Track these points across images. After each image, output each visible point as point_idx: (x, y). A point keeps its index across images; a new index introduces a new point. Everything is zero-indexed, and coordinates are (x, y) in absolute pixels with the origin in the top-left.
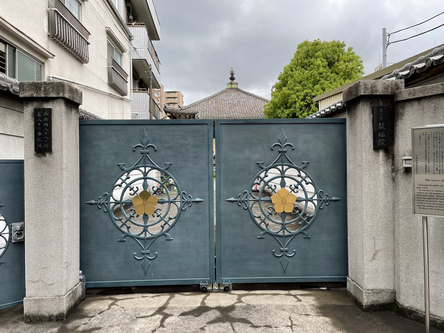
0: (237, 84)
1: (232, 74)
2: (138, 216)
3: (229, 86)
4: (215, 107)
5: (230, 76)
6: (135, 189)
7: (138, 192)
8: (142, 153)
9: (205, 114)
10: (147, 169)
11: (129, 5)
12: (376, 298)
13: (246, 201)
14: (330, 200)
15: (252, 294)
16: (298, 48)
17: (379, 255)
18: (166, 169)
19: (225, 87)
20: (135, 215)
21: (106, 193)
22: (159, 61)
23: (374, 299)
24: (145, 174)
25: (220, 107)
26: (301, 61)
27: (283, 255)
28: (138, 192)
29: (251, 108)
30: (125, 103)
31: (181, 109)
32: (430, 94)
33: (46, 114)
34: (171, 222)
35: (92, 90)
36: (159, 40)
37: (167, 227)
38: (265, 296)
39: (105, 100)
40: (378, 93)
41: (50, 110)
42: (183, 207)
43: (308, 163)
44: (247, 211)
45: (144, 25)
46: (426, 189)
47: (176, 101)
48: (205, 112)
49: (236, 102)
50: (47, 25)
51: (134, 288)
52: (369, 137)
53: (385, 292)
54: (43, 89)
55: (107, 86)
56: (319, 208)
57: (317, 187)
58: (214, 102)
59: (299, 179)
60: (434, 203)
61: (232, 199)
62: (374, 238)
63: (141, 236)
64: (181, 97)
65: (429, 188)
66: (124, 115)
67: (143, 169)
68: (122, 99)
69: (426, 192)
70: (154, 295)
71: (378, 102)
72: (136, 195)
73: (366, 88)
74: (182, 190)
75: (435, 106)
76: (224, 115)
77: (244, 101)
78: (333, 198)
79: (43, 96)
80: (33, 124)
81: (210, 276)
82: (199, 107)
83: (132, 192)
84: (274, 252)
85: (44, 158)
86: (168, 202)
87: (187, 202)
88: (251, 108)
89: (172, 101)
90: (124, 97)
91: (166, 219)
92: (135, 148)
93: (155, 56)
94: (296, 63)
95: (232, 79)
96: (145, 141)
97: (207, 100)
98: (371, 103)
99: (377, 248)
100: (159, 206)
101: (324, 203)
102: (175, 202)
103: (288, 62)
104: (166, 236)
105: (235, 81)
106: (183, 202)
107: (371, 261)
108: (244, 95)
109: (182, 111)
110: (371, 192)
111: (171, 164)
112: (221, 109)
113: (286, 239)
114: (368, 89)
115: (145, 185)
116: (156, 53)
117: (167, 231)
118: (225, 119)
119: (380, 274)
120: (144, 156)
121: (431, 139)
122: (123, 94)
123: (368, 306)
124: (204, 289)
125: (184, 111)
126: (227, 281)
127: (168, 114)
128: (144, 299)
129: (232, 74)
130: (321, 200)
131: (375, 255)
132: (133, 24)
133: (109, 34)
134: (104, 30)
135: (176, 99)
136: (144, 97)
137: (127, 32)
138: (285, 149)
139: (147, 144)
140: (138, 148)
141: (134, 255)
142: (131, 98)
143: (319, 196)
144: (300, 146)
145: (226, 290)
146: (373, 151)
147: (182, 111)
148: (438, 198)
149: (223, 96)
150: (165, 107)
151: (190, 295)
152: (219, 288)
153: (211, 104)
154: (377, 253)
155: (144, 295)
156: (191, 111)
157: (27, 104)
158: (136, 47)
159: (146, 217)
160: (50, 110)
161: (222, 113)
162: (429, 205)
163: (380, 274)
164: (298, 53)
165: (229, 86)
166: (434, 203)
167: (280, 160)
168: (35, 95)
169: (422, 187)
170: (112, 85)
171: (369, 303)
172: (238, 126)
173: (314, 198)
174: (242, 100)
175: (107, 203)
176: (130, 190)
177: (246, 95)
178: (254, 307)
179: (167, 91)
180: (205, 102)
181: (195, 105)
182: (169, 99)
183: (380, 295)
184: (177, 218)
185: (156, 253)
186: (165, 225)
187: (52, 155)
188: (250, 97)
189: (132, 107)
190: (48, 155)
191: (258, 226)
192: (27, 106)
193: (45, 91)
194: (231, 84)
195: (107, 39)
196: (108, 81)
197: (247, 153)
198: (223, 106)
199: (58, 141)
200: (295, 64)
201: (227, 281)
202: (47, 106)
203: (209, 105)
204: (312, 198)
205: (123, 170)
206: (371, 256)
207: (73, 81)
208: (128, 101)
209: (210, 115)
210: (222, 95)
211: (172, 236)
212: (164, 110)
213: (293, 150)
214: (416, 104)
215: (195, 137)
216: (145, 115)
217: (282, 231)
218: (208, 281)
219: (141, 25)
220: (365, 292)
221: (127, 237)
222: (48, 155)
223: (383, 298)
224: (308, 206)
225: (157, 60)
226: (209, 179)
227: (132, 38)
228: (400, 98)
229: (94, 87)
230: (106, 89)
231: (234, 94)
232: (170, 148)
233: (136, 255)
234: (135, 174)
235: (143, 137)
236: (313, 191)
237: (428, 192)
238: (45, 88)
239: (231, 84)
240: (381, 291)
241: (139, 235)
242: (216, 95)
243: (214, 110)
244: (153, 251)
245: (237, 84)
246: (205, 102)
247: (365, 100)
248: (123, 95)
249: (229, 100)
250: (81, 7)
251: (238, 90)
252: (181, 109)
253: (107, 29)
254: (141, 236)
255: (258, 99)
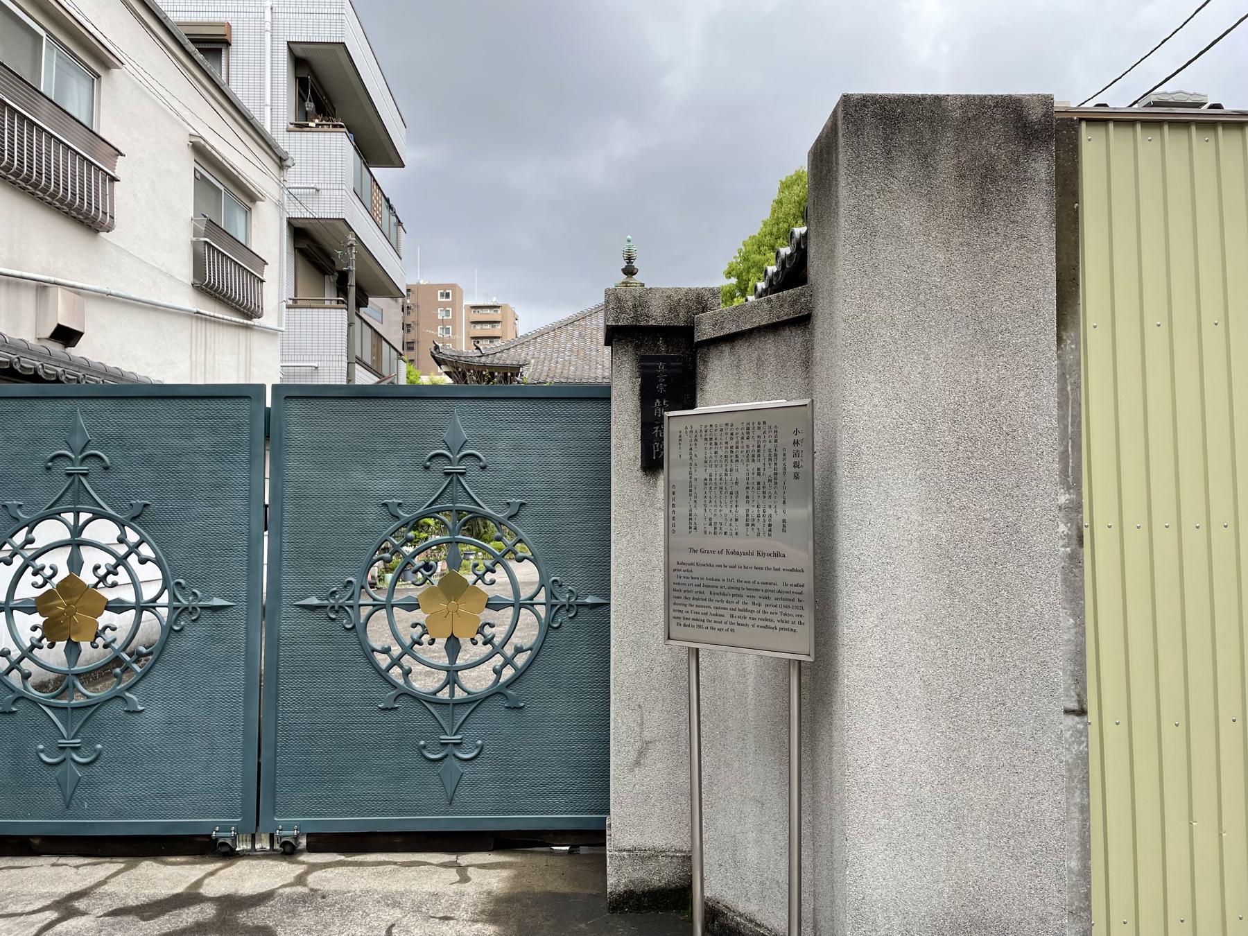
1: (629, 259)
2: (432, 642)
4: (575, 349)
6: (48, 572)
7: (56, 580)
8: (447, 474)
10: (84, 517)
11: (304, 74)
12: (641, 873)
13: (351, 607)
14: (579, 605)
15: (361, 864)
16: (781, 191)
17: (652, 755)
18: (510, 518)
20: (426, 638)
21: (350, 579)
22: (399, 223)
23: (636, 875)
24: (77, 530)
26: (786, 225)
27: (446, 756)
28: (56, 580)
30: (255, 338)
31: (483, 355)
32: (748, 327)
34: (521, 660)
35: (129, 304)
36: (403, 166)
37: (508, 673)
38: (380, 868)
39: (183, 331)
40: (652, 323)
42: (175, 623)
43: (522, 504)
44: (352, 635)
45: (341, 127)
46: (689, 574)
47: (497, 330)
51: (37, 842)
52: (631, 436)
53: (667, 856)
55: (189, 291)
56: (549, 625)
57: (543, 570)
58: (576, 334)
59: (122, 550)
60: (705, 610)
61: (314, 601)
62: (639, 706)
63: (440, 695)
64: (511, 320)
65: (697, 572)
66: (253, 369)
67: (69, 517)
68: (247, 327)
69: (690, 581)
70: (87, 860)
71: (655, 345)
72: (48, 587)
73: (620, 308)
74: (176, 575)
75: (759, 359)
76: (599, 371)
78: (589, 600)
81: (243, 814)
83: (39, 580)
84: (424, 747)
86: (513, 605)
87: (187, 608)
89: (487, 330)
90: (255, 322)
91: (509, 650)
92: (430, 460)
93: (386, 211)
94: (775, 230)
96: (78, 442)
97: (556, 329)
98: (637, 347)
99: (647, 735)
100: (488, 615)
101: (563, 611)
102: (532, 605)
103: (756, 229)
104: (125, 700)
105: (637, 278)
106: (176, 608)
107: (631, 770)
109: (483, 360)
110: (634, 581)
111: (146, 505)
113: (458, 710)
114: (625, 312)
115: (75, 564)
116: (388, 201)
117: (510, 684)
118: (599, 380)
119: (654, 805)
120: (73, 481)
121: (701, 441)
122: (248, 312)
123: (619, 895)
124: (225, 849)
125: (488, 361)
126: (288, 826)
127: (445, 368)
128: (54, 869)
129: (630, 259)
130: (554, 606)
131: (642, 753)
132: (311, 124)
133: (200, 151)
134: (184, 141)
135: (499, 326)
136: (331, 321)
137: (269, 146)
138: (461, 467)
139: (460, 450)
140: (59, 462)
141: (38, 752)
142: (280, 324)
143: (551, 595)
144: (502, 458)
145: (288, 851)
146: (640, 474)
147: (483, 360)
148: (712, 597)
150: (436, 347)
151: (181, 863)
152: (253, 845)
154: (647, 749)
155: (62, 860)
156: (508, 359)
158: (319, 186)
159: (453, 646)
161: (593, 365)
162: (763, 616)
163: (654, 805)
164: (780, 202)
166: (705, 610)
167: (447, 496)
169: (683, 567)
170: (205, 288)
171: (622, 888)
172: (331, 402)
173: (536, 600)
175: (351, 607)
176: (35, 574)
178: (324, 897)
179: (474, 304)
180: (551, 334)
182: (478, 327)
183: (652, 865)
184: (538, 651)
185: (99, 746)
186: (503, 666)
189: (291, 344)
191: (383, 675)
195: (194, 165)
196: (194, 276)
197: (359, 476)
200: (771, 234)
201: (289, 824)
204: (531, 599)
205: (17, 519)
206: (633, 755)
207: (53, 279)
208: (265, 331)
209: (559, 371)
211: (143, 701)
212: (434, 357)
213: (483, 468)
214: (726, 349)
215: (215, 431)
216: (333, 374)
217: (447, 690)
218: (237, 827)
219: (335, 126)
220: (611, 857)
221: (21, 703)
223: (660, 875)
224: (808, 616)
225: (394, 219)
226: (249, 547)
227: (289, 163)
228: (699, 337)
229: (134, 296)
230: (189, 301)
232: (148, 460)
233: (42, 751)
234: (50, 531)
235: (73, 431)
236: (535, 577)
237: (695, 582)
240: (655, 854)
241: (435, 694)
243: (573, 358)
244: (90, 743)
246: (551, 334)
247: (619, 340)
248: (250, 318)
250: (100, 83)
252: (483, 355)
253: (194, 140)
254: (440, 695)
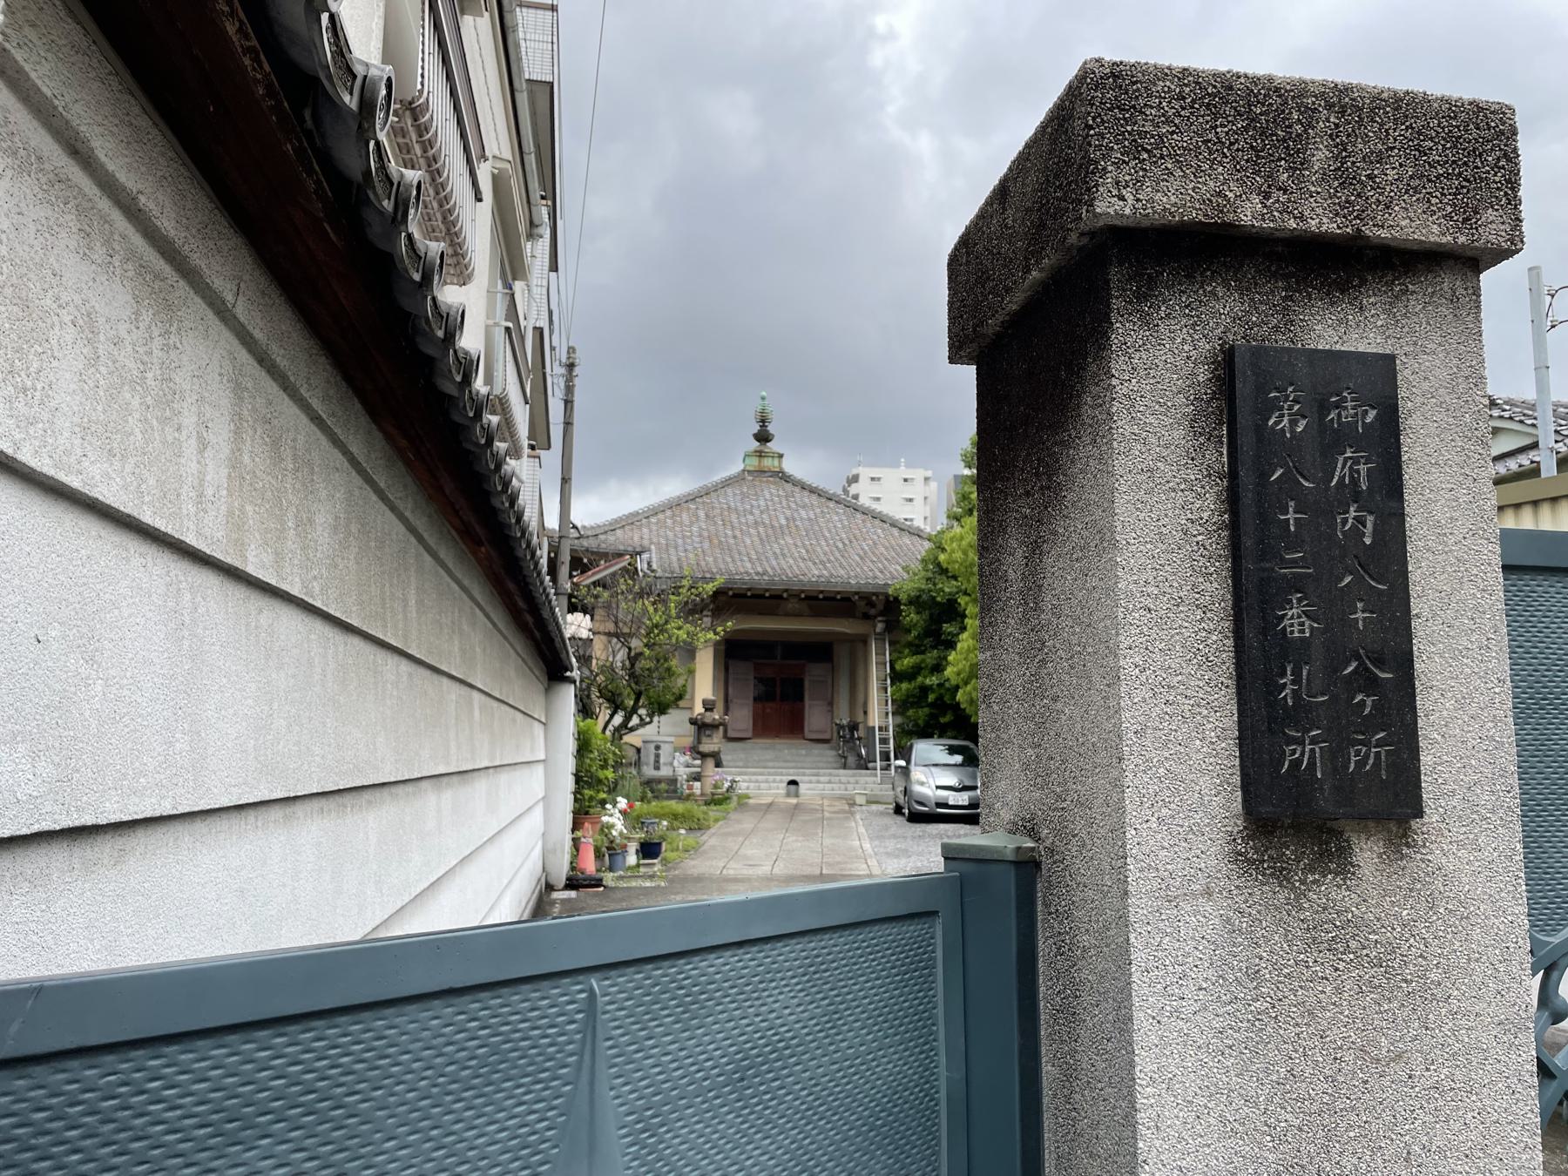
0: (781, 456)
1: (763, 421)
3: (753, 463)
4: (705, 534)
5: (756, 428)
9: (674, 559)
19: (736, 467)
25: (726, 536)
29: (840, 545)
33: (1354, 413)
41: (1387, 364)
48: (672, 551)
49: (783, 522)
50: (380, 45)
54: (1320, 155)
58: (702, 514)
77: (810, 519)
79: (1330, 226)
80: (1208, 505)
82: (645, 530)
85: (1328, 891)
88: (840, 545)
95: (763, 437)
97: (675, 505)
105: (773, 446)
108: (807, 498)
112: (732, 541)
129: (763, 421)
147: (585, 543)
149: (731, 496)
153: (692, 523)
157: (1141, 297)
160: (1379, 379)
165: (753, 463)
168: (1249, 213)
174: (803, 513)
177: (814, 497)
180: (669, 513)
181: (631, 521)
187: (1414, 864)
188: (832, 504)
190: (1367, 853)
192: (1146, 322)
193: (1343, 175)
194: (760, 454)
198: (738, 533)
199: (1461, 705)
202: (1338, 330)
203: (681, 523)
210: (729, 491)
222: (1367, 853)
231: (771, 492)
238: (1341, 150)
239: (760, 454)
242: (706, 492)
245: (781, 456)
246: (669, 513)
249: (756, 512)
251: (785, 477)
255: (859, 515)
